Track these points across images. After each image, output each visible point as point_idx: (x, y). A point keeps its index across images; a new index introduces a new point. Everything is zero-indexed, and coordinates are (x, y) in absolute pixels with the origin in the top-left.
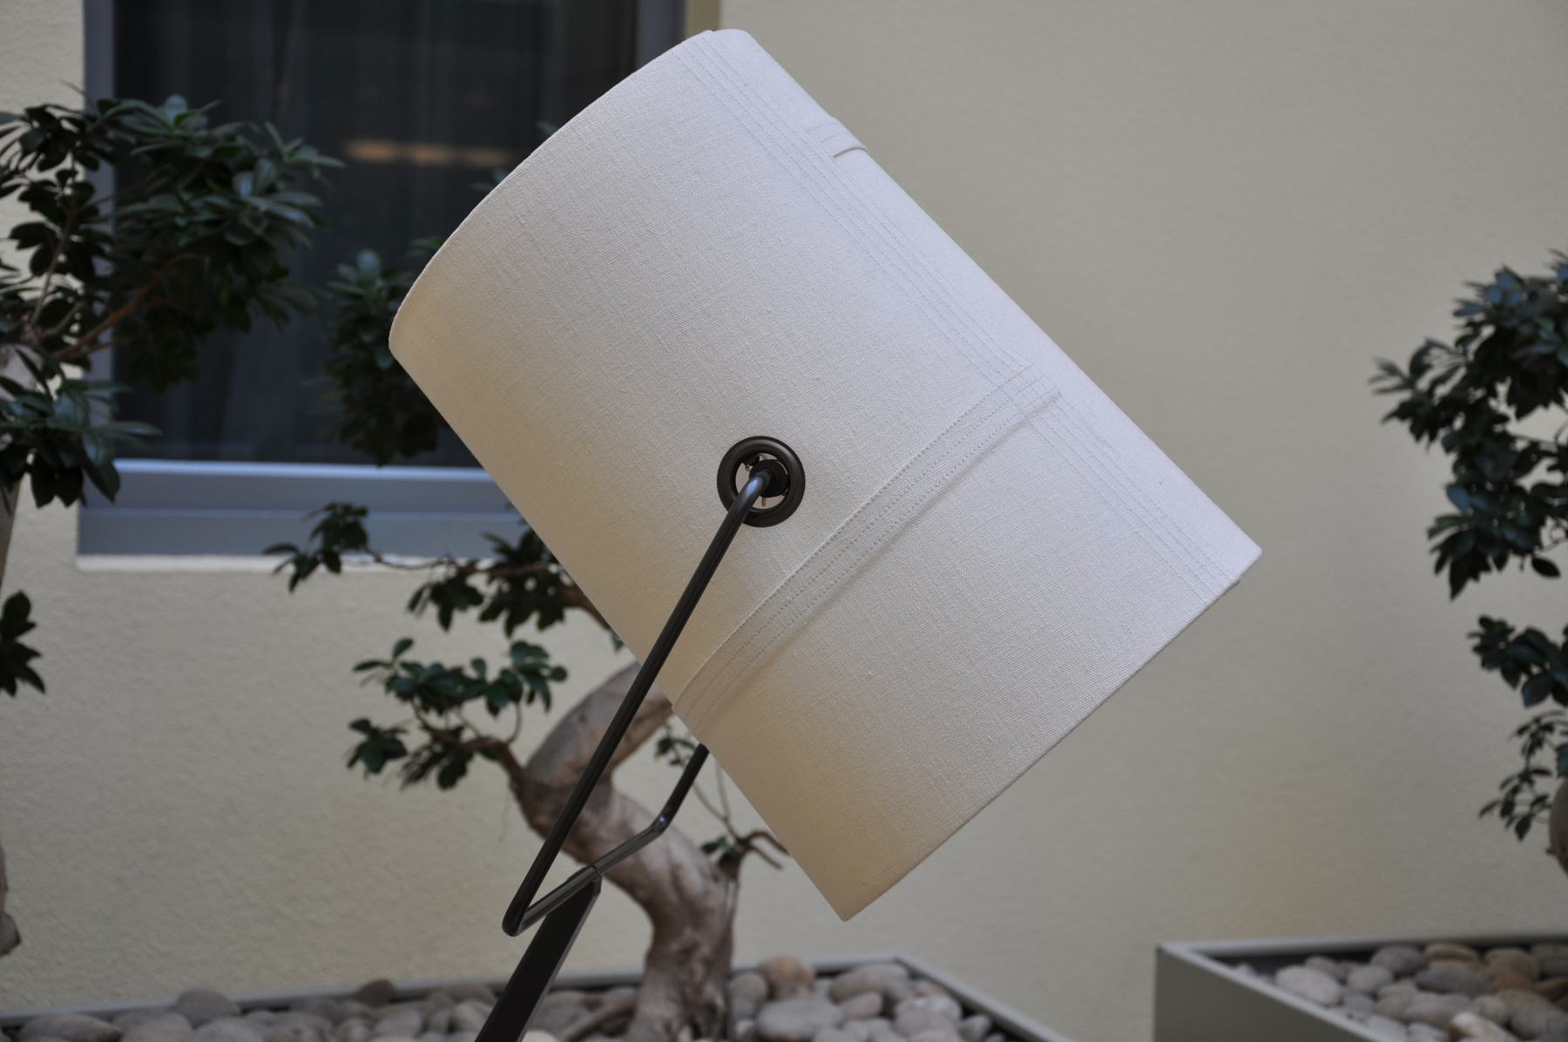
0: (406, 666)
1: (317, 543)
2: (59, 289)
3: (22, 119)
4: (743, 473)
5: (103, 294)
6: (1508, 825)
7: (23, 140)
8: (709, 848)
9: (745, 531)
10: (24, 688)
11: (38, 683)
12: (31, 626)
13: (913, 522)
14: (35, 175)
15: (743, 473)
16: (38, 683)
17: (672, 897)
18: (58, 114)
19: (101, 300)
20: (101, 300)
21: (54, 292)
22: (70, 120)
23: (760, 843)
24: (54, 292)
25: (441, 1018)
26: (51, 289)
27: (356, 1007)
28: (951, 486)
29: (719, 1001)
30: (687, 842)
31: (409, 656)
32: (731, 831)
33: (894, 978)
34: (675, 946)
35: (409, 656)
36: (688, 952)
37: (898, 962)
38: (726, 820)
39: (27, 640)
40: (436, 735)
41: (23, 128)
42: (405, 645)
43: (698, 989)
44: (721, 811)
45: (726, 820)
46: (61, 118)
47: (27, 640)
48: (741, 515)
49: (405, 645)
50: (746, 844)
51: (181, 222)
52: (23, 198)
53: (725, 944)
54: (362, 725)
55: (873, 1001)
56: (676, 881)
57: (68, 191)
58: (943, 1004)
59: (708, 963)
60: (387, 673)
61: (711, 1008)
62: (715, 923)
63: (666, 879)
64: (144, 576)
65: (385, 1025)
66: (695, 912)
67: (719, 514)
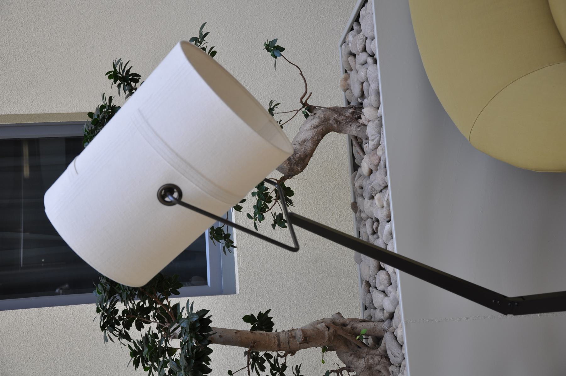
0: (255, 216)
1: (223, 241)
2: (154, 318)
3: (105, 332)
4: (167, 199)
5: (154, 305)
6: (137, 340)
7: (112, 332)
8: (307, 116)
9: (183, 200)
10: (269, 315)
11: (268, 311)
12: (252, 315)
13: (177, 154)
14: (121, 327)
15: (167, 199)
16: (268, 311)
17: (321, 128)
18: (102, 324)
19: (156, 306)
20: (156, 306)
21: (155, 319)
22: (104, 320)
23: (304, 101)
24: (155, 319)
25: (359, 191)
26: (154, 320)
27: (358, 213)
28: (166, 144)
29: (351, 110)
30: (305, 123)
31: (252, 215)
32: (301, 109)
33: (344, 49)
34: (335, 126)
35: (252, 215)
36: (337, 122)
37: (341, 46)
38: (298, 111)
39: (256, 316)
40: (278, 198)
41: (108, 332)
42: (249, 216)
43: (347, 117)
44: (296, 111)
45: (298, 111)
46: (103, 322)
47: (256, 316)
48: (179, 201)
49: (249, 216)
50: (305, 105)
51: (129, 293)
52: (129, 329)
53: (335, 110)
54: (274, 226)
55: (351, 59)
56: (316, 127)
57: (125, 317)
58: (350, 38)
59: (340, 115)
60: (257, 222)
61: (353, 113)
62: (328, 113)
63: (315, 130)
64: (240, 275)
65: (362, 209)
66: (325, 120)
67: (178, 206)
